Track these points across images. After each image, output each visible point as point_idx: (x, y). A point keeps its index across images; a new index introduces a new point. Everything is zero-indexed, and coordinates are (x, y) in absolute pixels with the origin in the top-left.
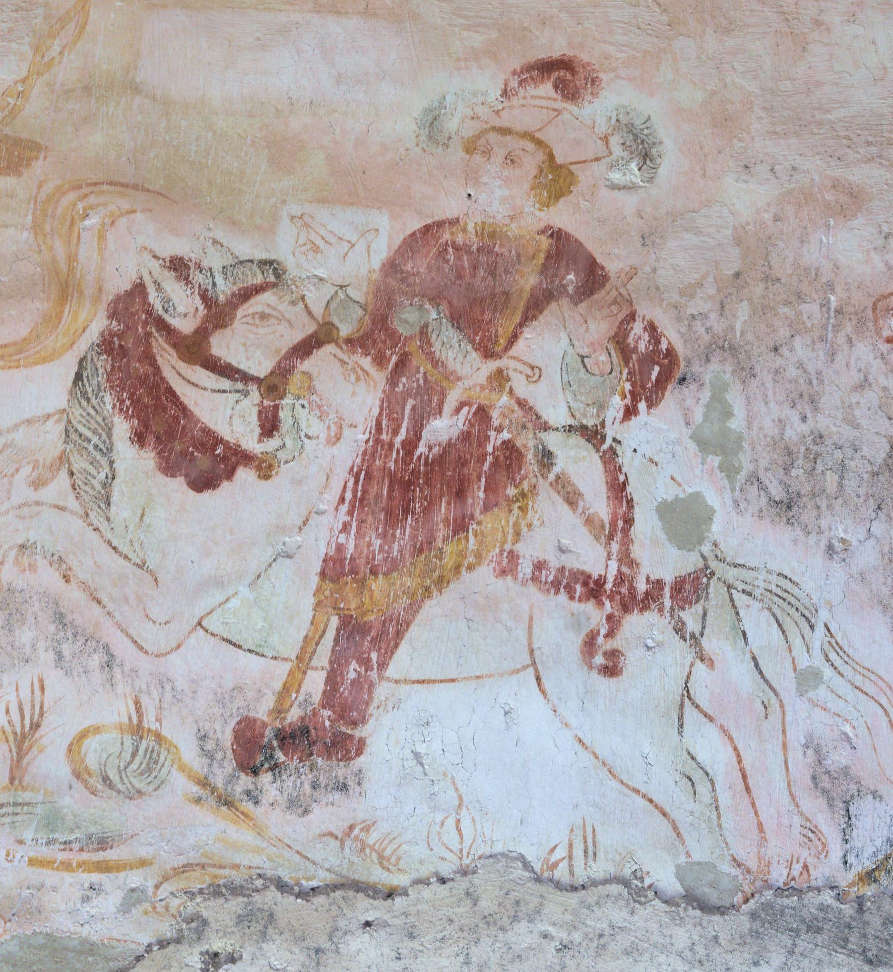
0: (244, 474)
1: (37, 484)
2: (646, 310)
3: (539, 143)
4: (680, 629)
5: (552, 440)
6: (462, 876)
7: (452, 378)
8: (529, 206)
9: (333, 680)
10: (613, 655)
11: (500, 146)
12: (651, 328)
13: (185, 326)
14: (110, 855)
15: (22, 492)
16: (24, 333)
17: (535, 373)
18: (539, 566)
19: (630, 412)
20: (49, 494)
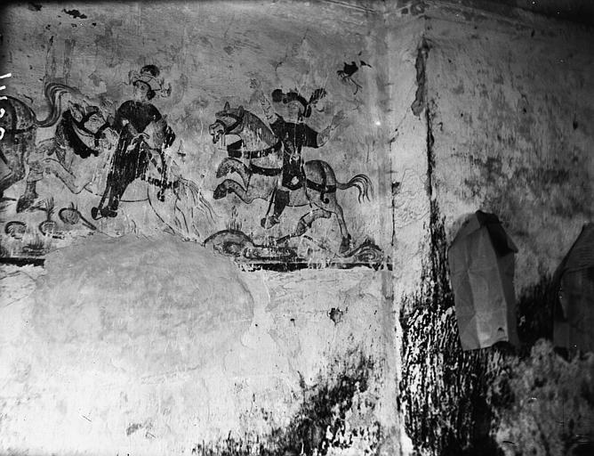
0: (92, 155)
1: (49, 154)
2: (169, 124)
3: (149, 85)
4: (175, 192)
5: (151, 151)
6: (225, 48)
7: (132, 137)
8: (146, 99)
9: (111, 200)
10: (163, 197)
11: (141, 85)
12: (170, 128)
13: (79, 121)
14: (181, 220)
15: (46, 156)
16: (44, 119)
17: (148, 137)
18: (149, 178)
19: (166, 147)
20: (52, 156)
